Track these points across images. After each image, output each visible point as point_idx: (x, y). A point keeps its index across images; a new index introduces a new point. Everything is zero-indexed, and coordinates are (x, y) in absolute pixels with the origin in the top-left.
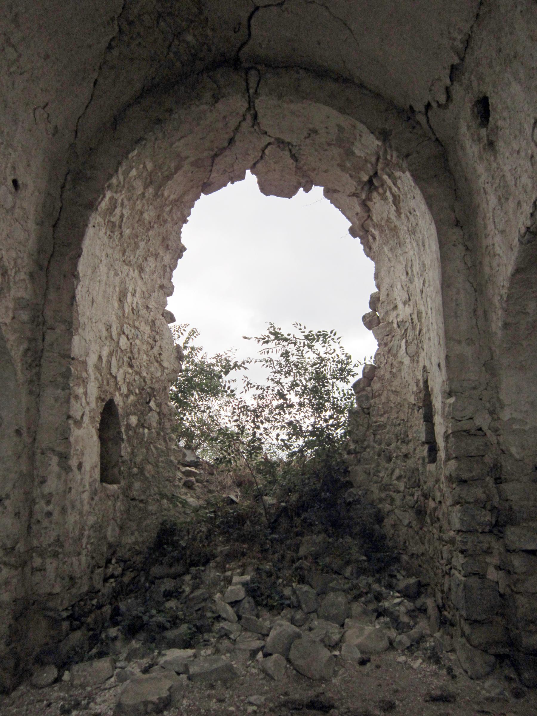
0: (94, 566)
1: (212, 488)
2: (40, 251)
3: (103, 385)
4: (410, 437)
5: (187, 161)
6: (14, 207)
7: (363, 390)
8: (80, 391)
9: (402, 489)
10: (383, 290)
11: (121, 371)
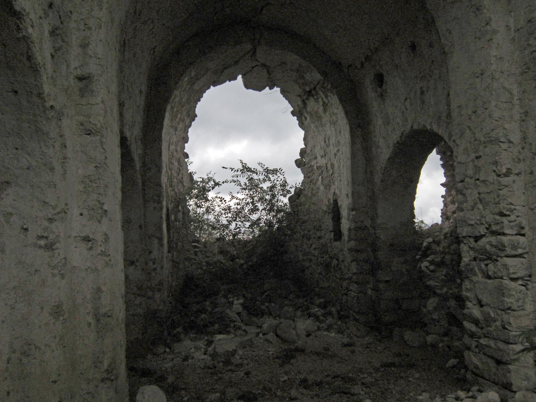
1: (208, 254)
4: (322, 228)
9: (316, 255)
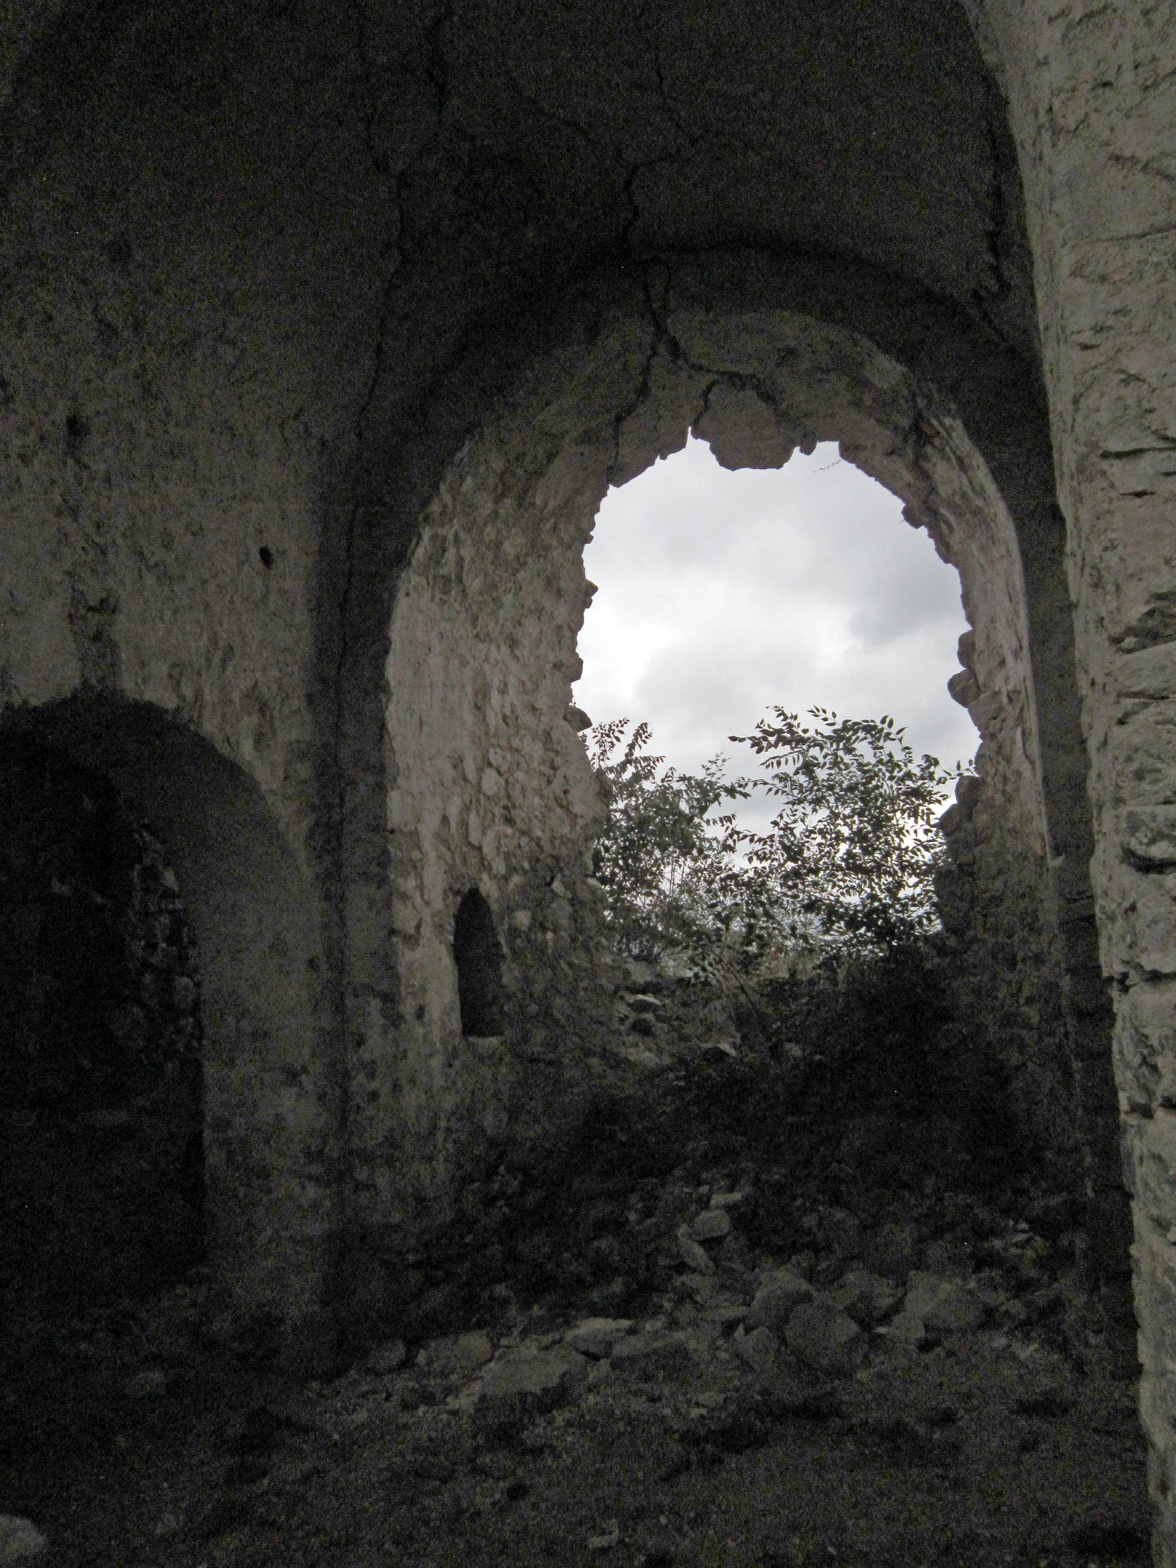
0: (463, 1179)
1: (688, 1030)
2: (321, 653)
3: (454, 865)
5: (567, 439)
6: (265, 597)
7: (958, 828)
8: (409, 885)
10: (980, 626)
11: (490, 835)
